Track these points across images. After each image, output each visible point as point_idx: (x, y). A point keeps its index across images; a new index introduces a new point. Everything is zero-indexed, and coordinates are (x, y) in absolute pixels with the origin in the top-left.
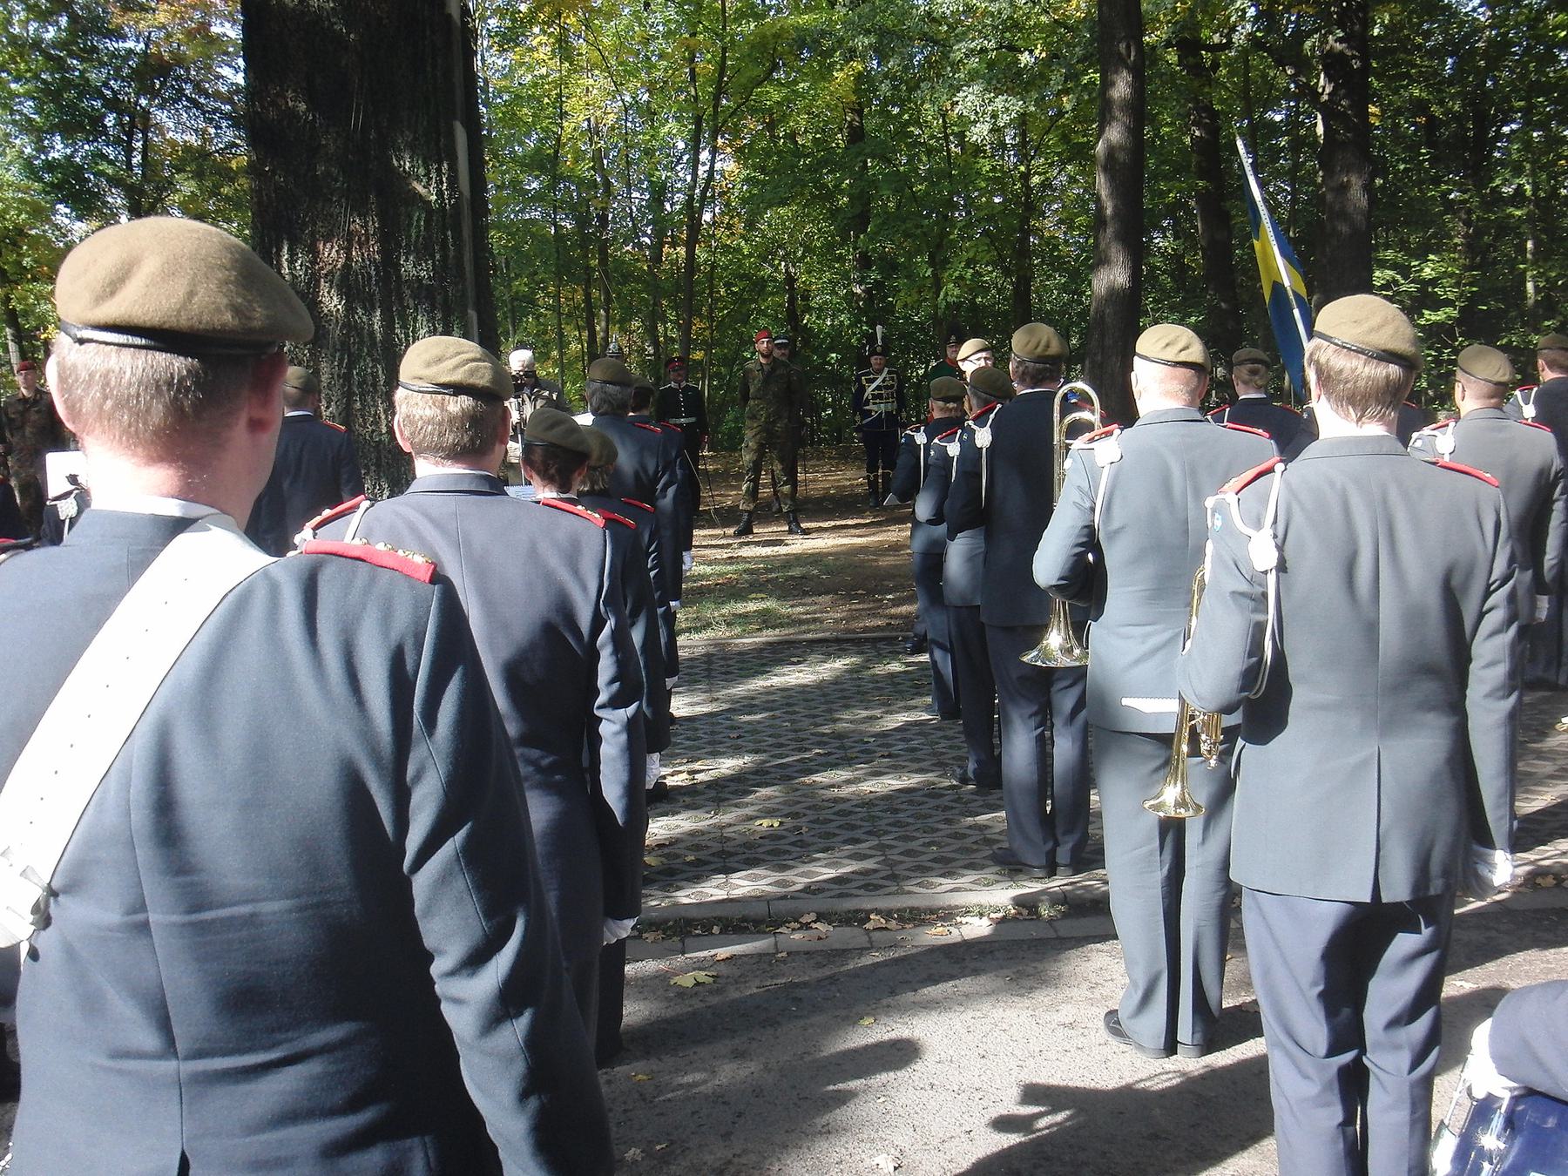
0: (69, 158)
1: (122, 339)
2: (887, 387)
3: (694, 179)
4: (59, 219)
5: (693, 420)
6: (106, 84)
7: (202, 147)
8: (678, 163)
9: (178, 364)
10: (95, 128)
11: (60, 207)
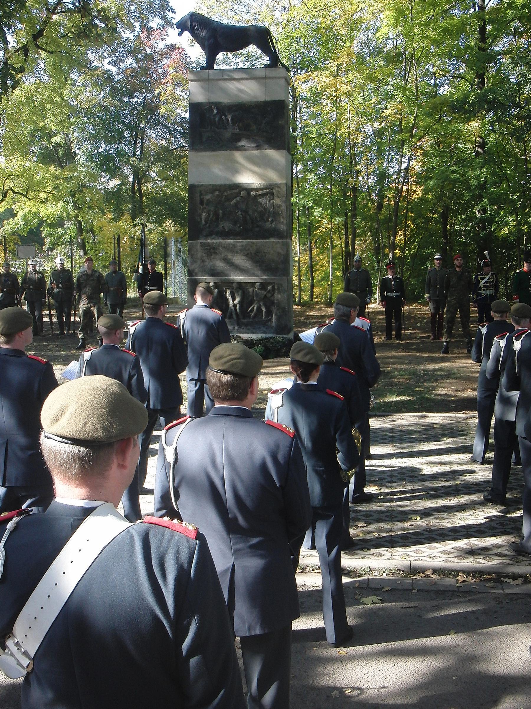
1: (61, 439)
2: (490, 282)
5: (398, 294)
7: (168, 147)
9: (82, 450)
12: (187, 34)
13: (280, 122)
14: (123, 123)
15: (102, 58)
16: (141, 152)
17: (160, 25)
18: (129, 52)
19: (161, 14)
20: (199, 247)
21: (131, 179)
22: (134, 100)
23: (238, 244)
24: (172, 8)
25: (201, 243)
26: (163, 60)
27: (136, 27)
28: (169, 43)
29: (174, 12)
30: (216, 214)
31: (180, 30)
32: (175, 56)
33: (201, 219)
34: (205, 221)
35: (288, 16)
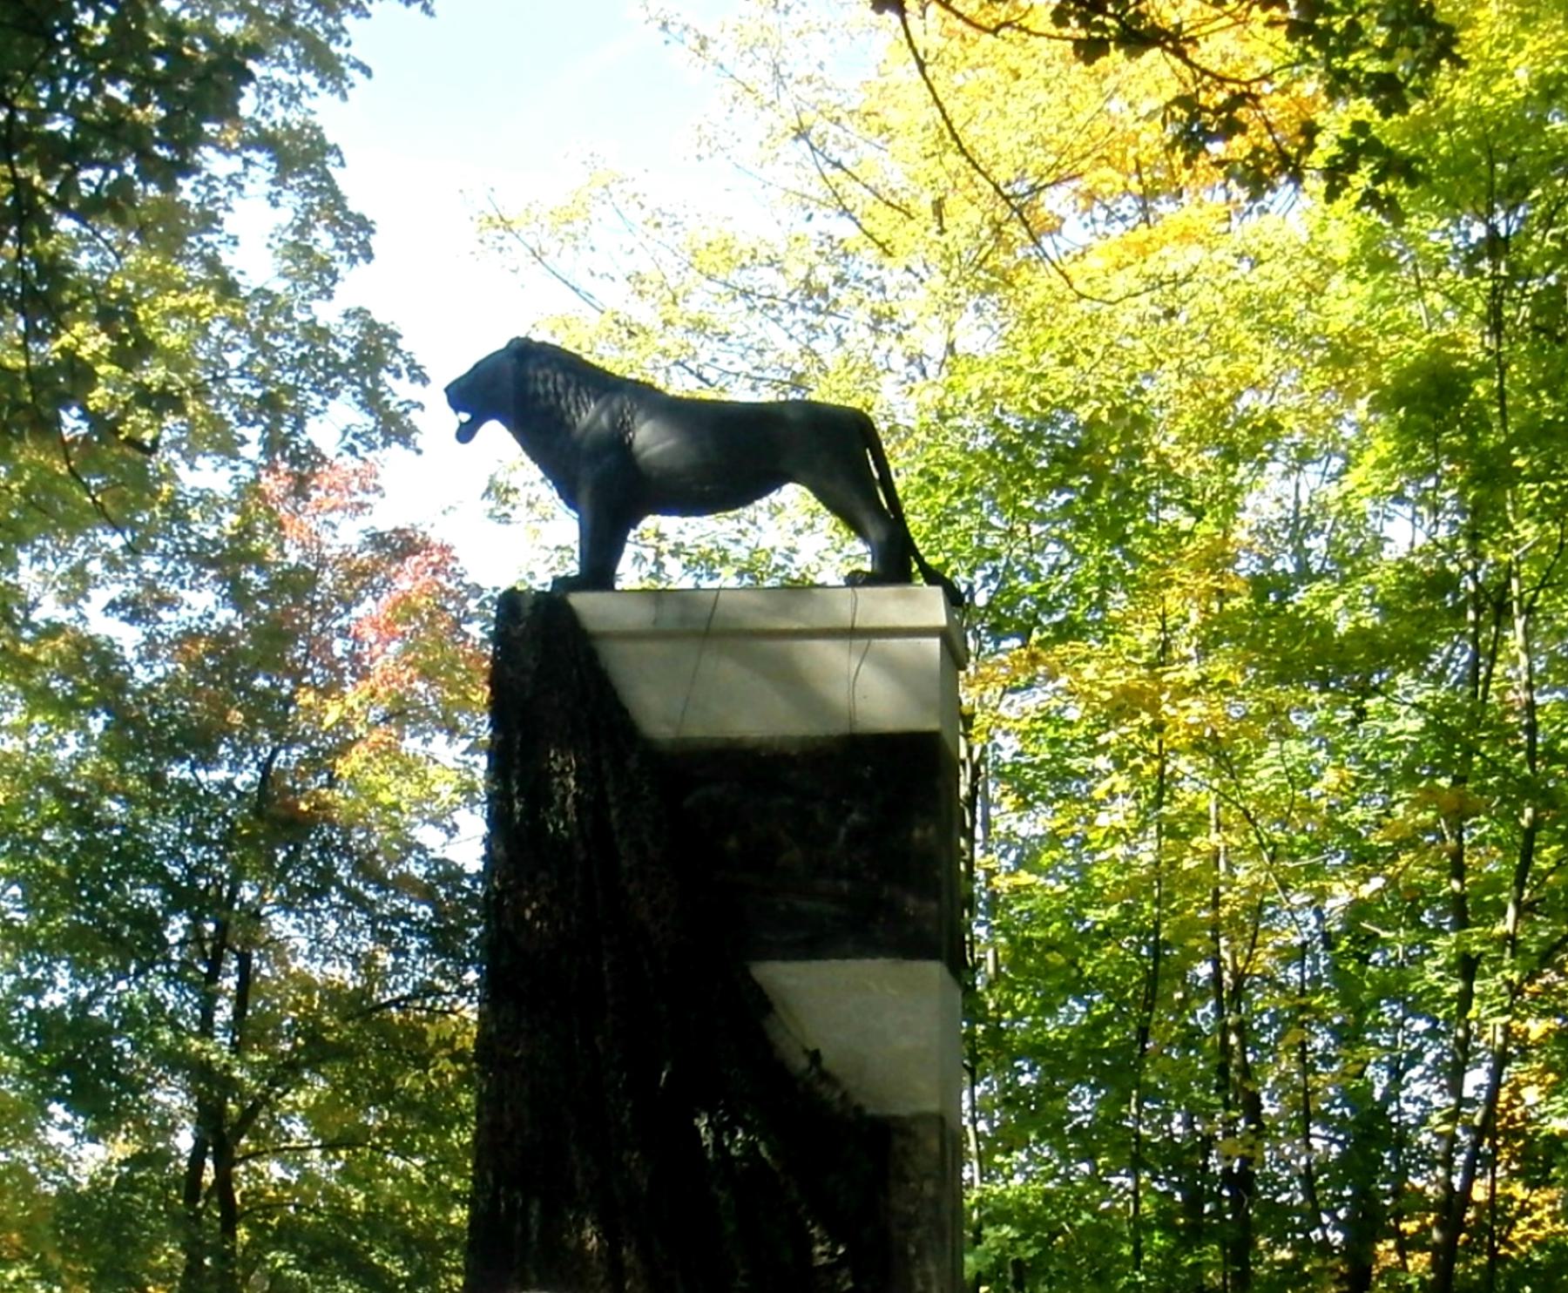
0: (80, 1006)
3: (244, 960)
4: (55, 1136)
6: (175, 854)
7: (364, 993)
8: (1411, 1064)
10: (138, 942)
11: (57, 1109)
12: (495, 434)
13: (917, 834)
14: (158, 876)
15: (78, 583)
16: (239, 1013)
17: (355, 436)
18: (201, 557)
19: (362, 385)
21: (185, 1141)
22: (221, 774)
24: (412, 366)
27: (244, 441)
28: (385, 526)
29: (418, 375)
31: (465, 417)
32: (408, 579)
35: (940, 392)
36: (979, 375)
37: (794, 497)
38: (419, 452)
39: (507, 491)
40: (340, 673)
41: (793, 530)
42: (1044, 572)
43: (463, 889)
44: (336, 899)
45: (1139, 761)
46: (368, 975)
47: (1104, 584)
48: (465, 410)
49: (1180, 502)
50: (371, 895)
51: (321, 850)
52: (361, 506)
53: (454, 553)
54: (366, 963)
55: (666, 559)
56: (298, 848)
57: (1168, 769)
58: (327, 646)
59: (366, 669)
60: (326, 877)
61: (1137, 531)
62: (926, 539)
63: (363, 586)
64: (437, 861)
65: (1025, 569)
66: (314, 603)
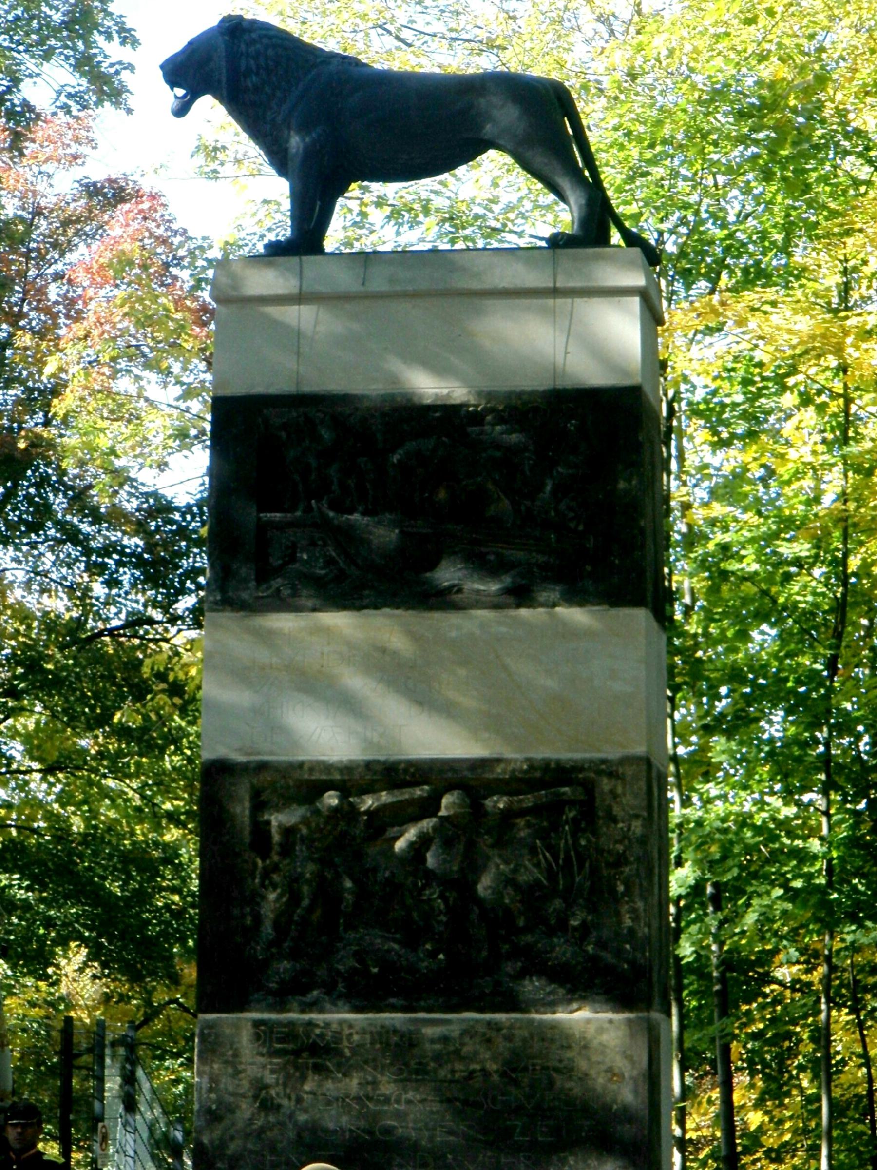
7: (79, 623)
12: (208, 107)
13: (622, 485)
17: (70, 96)
19: (74, 49)
20: (245, 1038)
23: (429, 1031)
25: (257, 1024)
26: (70, 246)
29: (128, 37)
30: (326, 893)
32: (121, 226)
33: (258, 919)
34: (276, 925)
36: (666, 36)
37: (494, 161)
38: (129, 111)
39: (215, 149)
40: (55, 316)
41: (494, 196)
42: (731, 218)
43: (172, 522)
44: (52, 532)
45: (824, 398)
46: (84, 606)
47: (789, 229)
48: (180, 86)
49: (860, 155)
50: (85, 528)
51: (38, 486)
52: (75, 157)
53: (163, 200)
54: (79, 594)
55: (371, 210)
56: (15, 485)
57: (853, 408)
58: (42, 292)
59: (79, 312)
60: (44, 510)
61: (818, 180)
62: (619, 190)
63: (76, 234)
64: (147, 495)
65: (713, 216)
66: (30, 251)
